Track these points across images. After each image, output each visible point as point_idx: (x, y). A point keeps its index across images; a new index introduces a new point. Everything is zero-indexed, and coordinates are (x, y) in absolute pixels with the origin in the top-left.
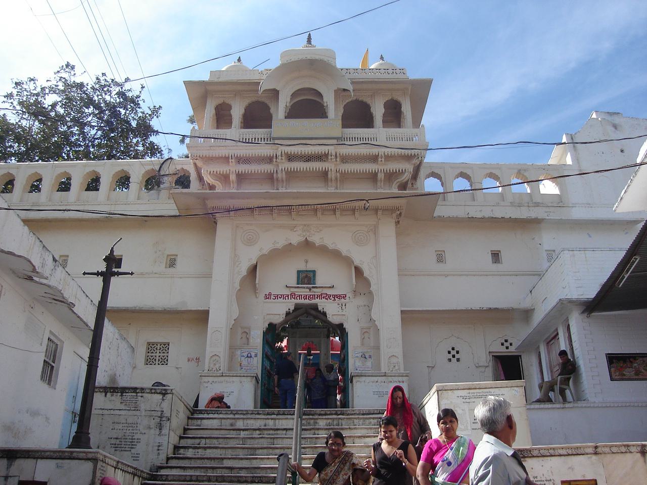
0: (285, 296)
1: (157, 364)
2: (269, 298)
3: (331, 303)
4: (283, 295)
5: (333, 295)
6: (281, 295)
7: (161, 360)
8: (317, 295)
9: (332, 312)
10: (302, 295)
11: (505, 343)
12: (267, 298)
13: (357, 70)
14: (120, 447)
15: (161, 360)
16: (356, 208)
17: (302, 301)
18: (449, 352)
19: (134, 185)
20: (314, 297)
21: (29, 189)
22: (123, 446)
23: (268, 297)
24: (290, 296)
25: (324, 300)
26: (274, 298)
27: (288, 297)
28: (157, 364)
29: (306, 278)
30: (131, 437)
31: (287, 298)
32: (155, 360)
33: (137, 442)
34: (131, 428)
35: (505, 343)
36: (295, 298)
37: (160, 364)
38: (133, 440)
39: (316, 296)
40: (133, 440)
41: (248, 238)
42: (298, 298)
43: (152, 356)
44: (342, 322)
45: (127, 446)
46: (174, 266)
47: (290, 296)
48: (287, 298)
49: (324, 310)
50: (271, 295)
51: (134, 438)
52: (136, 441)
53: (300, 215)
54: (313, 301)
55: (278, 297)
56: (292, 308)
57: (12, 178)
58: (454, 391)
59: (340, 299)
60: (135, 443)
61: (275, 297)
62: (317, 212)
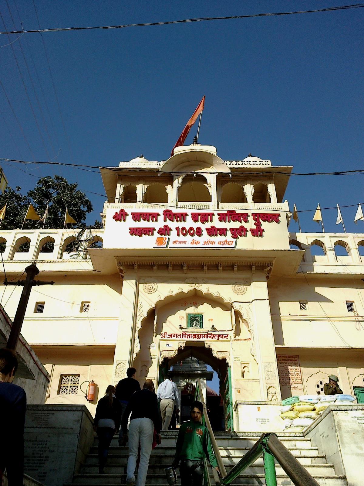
0: (177, 335)
1: (68, 393)
2: (164, 337)
3: (216, 341)
4: (176, 334)
5: (217, 335)
6: (175, 334)
7: (71, 390)
8: (204, 335)
9: (217, 348)
10: (191, 334)
11: (320, 385)
12: (163, 337)
13: (249, 162)
14: (28, 466)
15: (71, 390)
16: (253, 264)
17: (192, 339)
18: (318, 386)
19: (57, 249)
20: (201, 336)
21: (41, 249)
22: (31, 465)
23: (164, 336)
24: (181, 335)
25: (210, 339)
26: (169, 337)
27: (180, 336)
28: (68, 393)
29: (195, 320)
30: (39, 455)
31: (179, 337)
32: (67, 390)
33: (45, 460)
34: (40, 446)
35: (320, 385)
36: (186, 337)
37: (71, 393)
38: (42, 459)
39: (203, 335)
40: (42, 459)
41: (149, 287)
42: (189, 337)
43: (75, 384)
44: (137, 370)
45: (35, 465)
46: (87, 311)
47: (181, 335)
48: (179, 337)
49: (210, 347)
50: (166, 334)
51: (42, 456)
52: (44, 459)
53: (190, 270)
54: (201, 340)
55: (172, 336)
56: (184, 345)
57: (26, 241)
58: (348, 411)
59: (223, 338)
60: (43, 462)
61: (170, 336)
62: (203, 267)
